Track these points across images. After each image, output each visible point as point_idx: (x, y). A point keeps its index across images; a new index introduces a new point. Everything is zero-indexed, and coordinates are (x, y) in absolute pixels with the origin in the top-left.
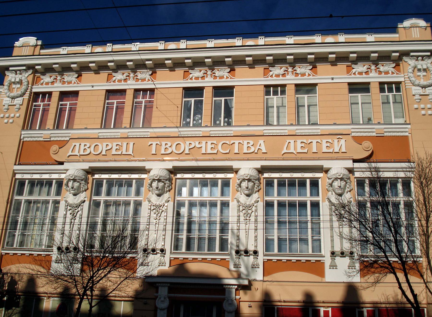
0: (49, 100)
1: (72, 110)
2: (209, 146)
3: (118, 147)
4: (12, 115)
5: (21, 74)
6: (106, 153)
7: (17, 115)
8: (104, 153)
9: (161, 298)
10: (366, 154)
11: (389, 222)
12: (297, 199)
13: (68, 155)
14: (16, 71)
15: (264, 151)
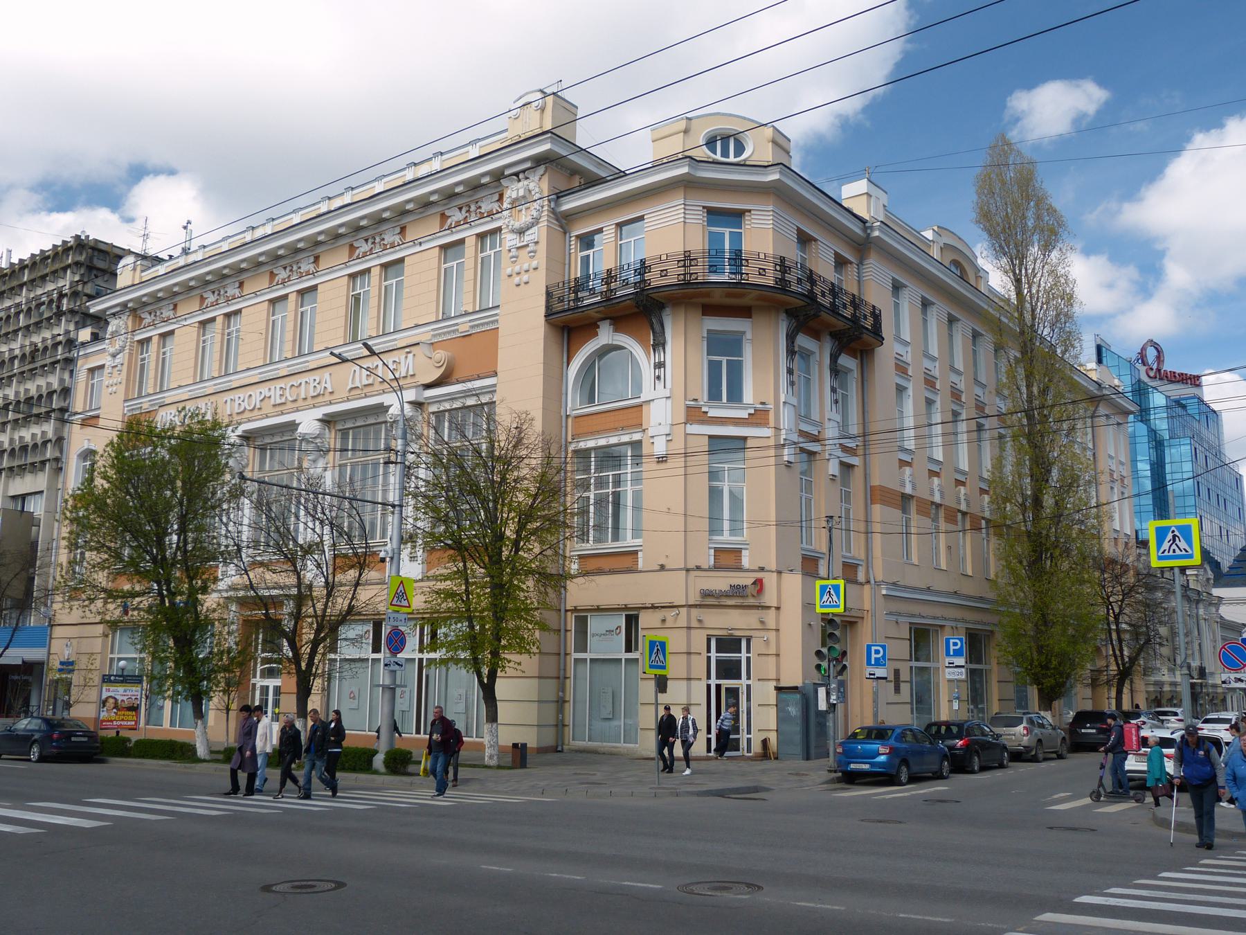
5: (527, 178)
10: (435, 375)
11: (169, 507)
13: (349, 388)
14: (517, 174)
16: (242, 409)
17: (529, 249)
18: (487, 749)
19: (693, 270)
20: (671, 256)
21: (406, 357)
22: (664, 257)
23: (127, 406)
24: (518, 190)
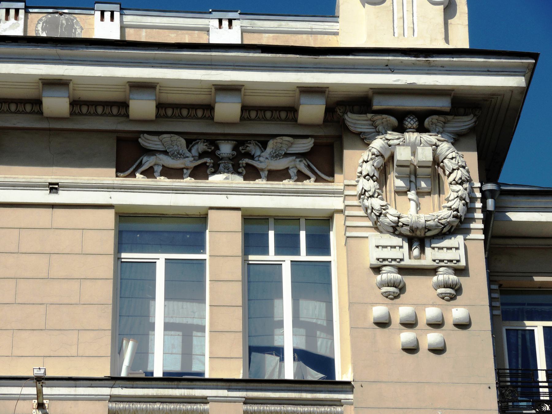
17: (435, 278)
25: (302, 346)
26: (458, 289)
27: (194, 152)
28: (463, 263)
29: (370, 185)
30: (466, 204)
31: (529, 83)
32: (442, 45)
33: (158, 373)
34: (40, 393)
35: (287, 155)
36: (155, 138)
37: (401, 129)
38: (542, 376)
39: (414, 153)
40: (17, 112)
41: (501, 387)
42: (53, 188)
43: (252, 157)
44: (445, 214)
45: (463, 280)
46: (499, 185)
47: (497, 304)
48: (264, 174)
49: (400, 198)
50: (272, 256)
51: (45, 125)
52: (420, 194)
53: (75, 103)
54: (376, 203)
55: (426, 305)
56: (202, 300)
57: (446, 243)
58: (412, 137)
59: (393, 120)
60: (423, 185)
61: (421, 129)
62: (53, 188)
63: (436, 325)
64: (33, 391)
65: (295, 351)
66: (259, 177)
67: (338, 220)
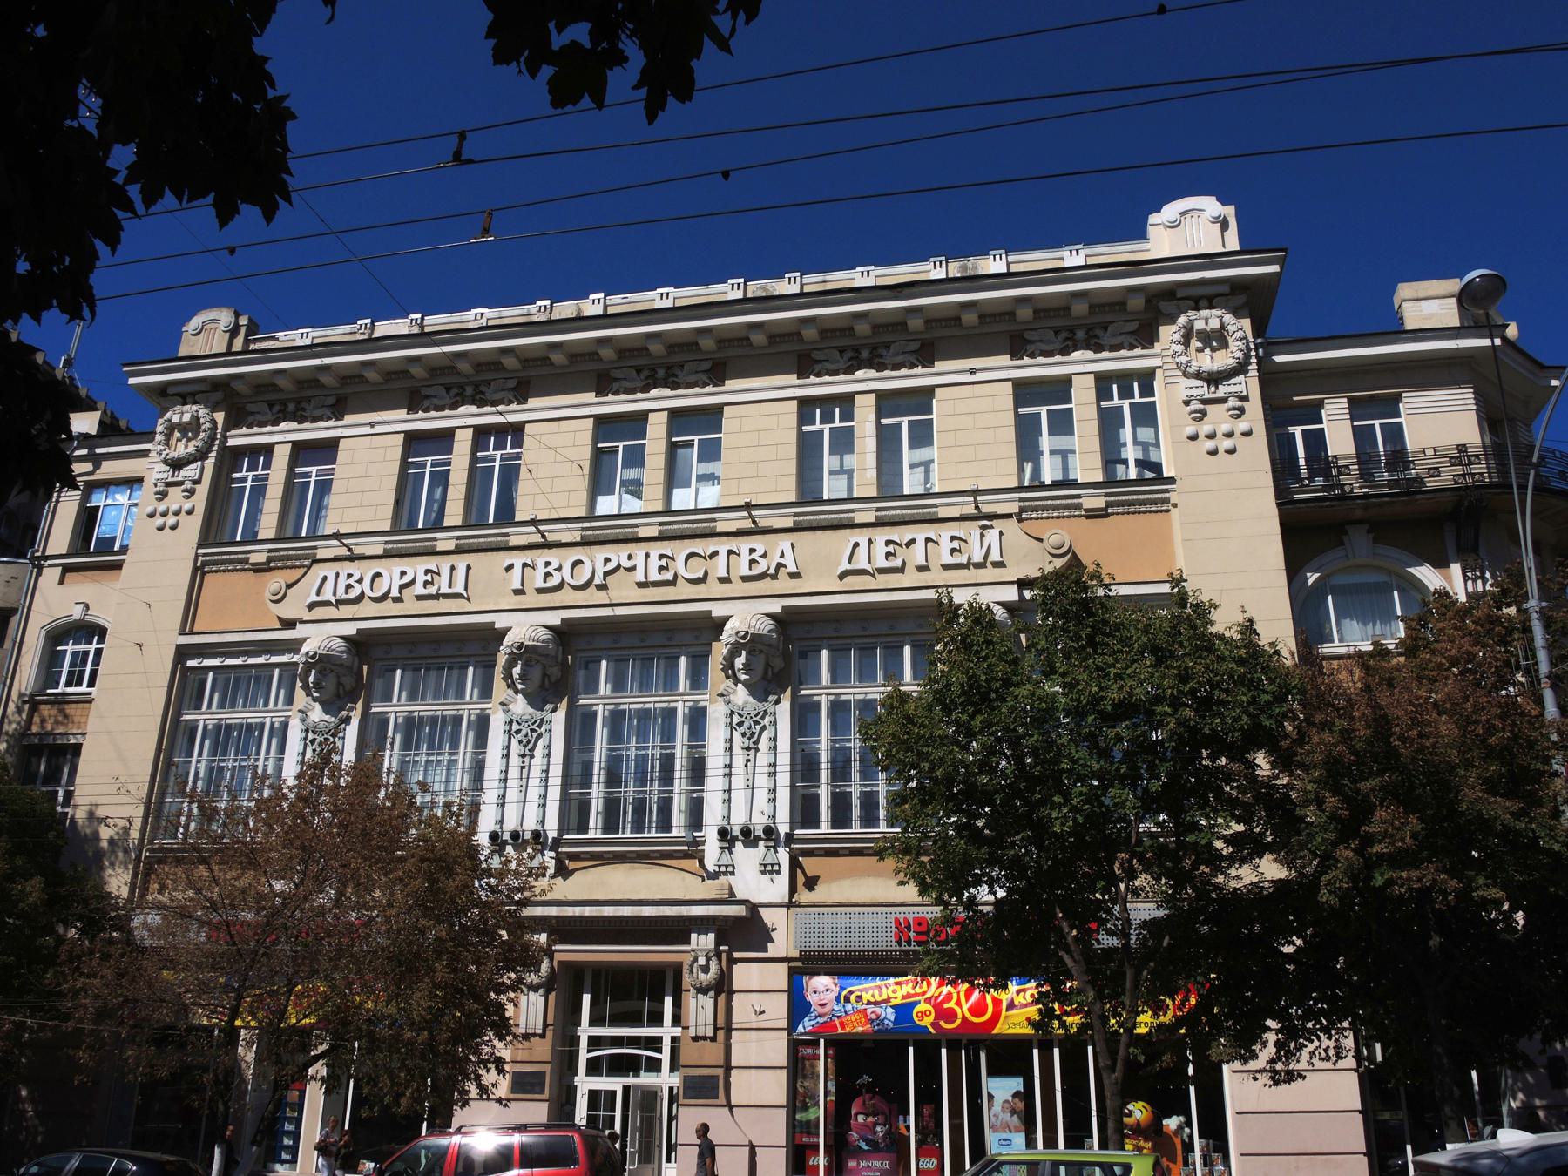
0: (848, 415)
1: (324, 487)
2: (654, 563)
3: (429, 578)
4: (174, 507)
6: (1002, 557)
7: (187, 506)
8: (598, 580)
9: (700, 959)
12: (655, 701)
15: (792, 569)
16: (353, 594)
17: (183, 487)
18: (1174, 1139)
19: (1475, 469)
20: (1442, 450)
21: (982, 535)
22: (1430, 452)
23: (204, 555)
24: (182, 413)
25: (1140, 457)
26: (1242, 410)
27: (642, 377)
28: (1245, 393)
29: (1180, 348)
30: (1244, 354)
31: (1282, 268)
32: (1221, 250)
33: (1048, 482)
34: (976, 501)
35: (1121, 334)
36: (1034, 333)
37: (1197, 309)
38: (1302, 462)
39: (1207, 324)
40: (946, 326)
41: (1274, 472)
42: (973, 372)
43: (881, 357)
44: (1231, 362)
45: (1245, 404)
46: (1266, 339)
47: (1269, 418)
48: (890, 367)
49: (1200, 355)
50: (1116, 402)
51: (965, 332)
52: (1213, 350)
53: (927, 322)
54: (1184, 359)
55: (1221, 423)
56: (1072, 433)
57: (1233, 381)
58: (1205, 313)
59: (180, 399)
60: (1215, 344)
61: (1211, 307)
62: (973, 372)
63: (1229, 435)
64: (972, 499)
65: (1136, 460)
66: (886, 369)
67: (1158, 372)
